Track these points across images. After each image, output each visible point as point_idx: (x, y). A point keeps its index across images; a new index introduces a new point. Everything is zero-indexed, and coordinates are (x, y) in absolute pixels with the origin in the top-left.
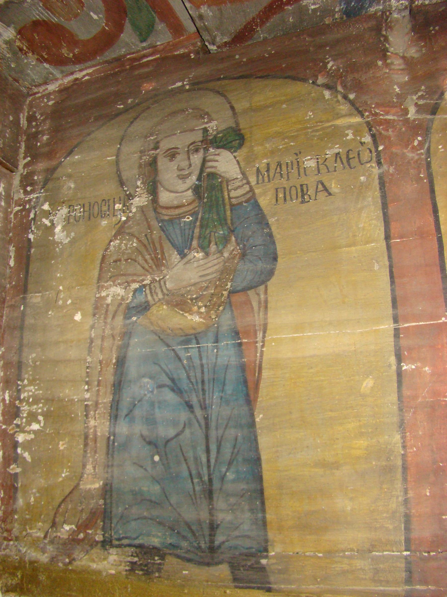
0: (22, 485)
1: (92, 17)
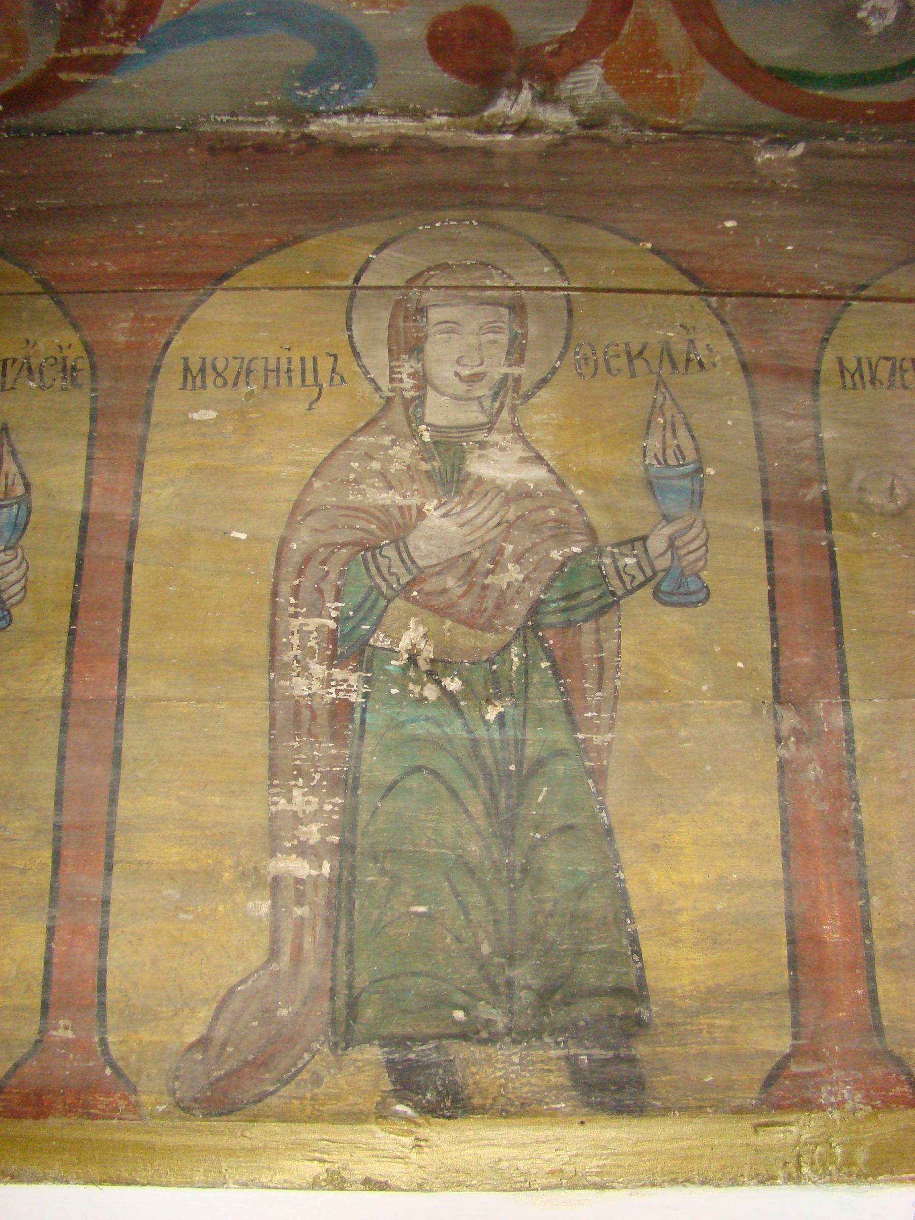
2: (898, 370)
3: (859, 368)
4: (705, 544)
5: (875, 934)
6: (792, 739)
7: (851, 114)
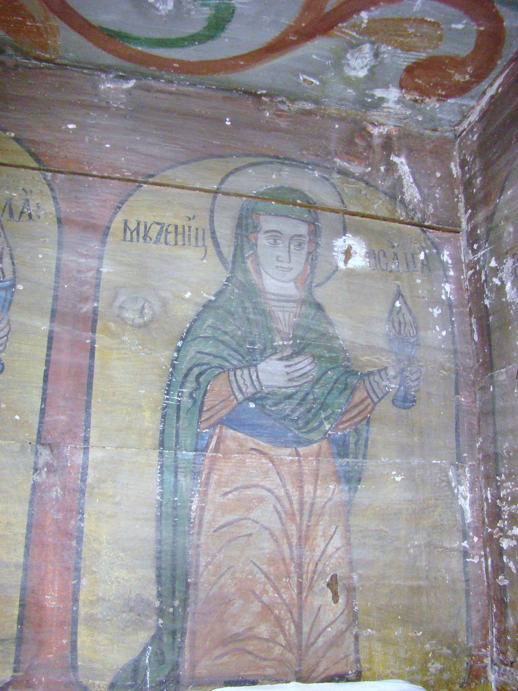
0: (510, 600)
1: (457, 30)
2: (164, 232)
3: (138, 229)
4: (7, 335)
5: (80, 603)
6: (45, 469)
7: (165, 64)
